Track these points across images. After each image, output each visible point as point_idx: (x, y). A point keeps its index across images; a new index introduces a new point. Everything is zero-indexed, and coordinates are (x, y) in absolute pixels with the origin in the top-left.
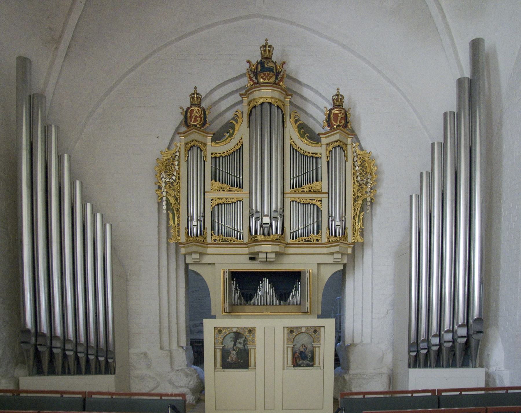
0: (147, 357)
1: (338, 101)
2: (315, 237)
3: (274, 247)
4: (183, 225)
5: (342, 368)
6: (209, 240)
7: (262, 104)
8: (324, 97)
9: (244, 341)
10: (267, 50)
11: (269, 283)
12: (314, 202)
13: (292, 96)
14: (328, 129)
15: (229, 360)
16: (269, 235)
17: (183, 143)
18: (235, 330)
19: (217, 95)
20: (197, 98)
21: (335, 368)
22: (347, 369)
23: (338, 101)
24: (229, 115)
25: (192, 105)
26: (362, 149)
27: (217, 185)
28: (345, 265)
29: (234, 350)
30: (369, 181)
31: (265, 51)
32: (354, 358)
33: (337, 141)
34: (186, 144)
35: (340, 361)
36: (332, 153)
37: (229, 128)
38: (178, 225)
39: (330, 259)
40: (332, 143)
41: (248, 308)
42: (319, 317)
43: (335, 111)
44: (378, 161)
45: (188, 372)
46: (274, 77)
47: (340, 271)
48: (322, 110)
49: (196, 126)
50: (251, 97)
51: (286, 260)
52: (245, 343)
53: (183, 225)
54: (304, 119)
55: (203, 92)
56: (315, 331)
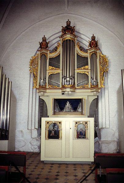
0: (22, 132)
1: (93, 38)
2: (86, 86)
3: (71, 89)
4: (38, 82)
5: (98, 138)
6: (47, 87)
7: (67, 40)
8: (88, 38)
9: (57, 127)
10: (68, 23)
11: (69, 103)
12: (86, 73)
13: (77, 37)
14: (90, 48)
15: (51, 135)
16: (69, 85)
17: (39, 54)
18: (54, 122)
19: (52, 38)
20: (45, 39)
21: (94, 139)
22: (100, 138)
23: (93, 38)
24: (56, 45)
25: (43, 41)
26: (103, 54)
27: (51, 67)
28: (98, 96)
29: (53, 131)
30: (106, 65)
31: (68, 23)
32: (103, 133)
33: (93, 52)
34: (40, 54)
35: (97, 134)
36: (92, 56)
37: (56, 49)
38: (37, 82)
39: (92, 94)
40: (91, 52)
41: (61, 113)
42: (88, 117)
43: (93, 41)
44: (109, 59)
45: (38, 139)
46: (71, 31)
47: (96, 99)
48: (88, 42)
49: (44, 48)
50: (63, 38)
51: (76, 94)
52: (58, 127)
53: (38, 82)
54: (81, 45)
55: (47, 37)
56: (86, 123)
